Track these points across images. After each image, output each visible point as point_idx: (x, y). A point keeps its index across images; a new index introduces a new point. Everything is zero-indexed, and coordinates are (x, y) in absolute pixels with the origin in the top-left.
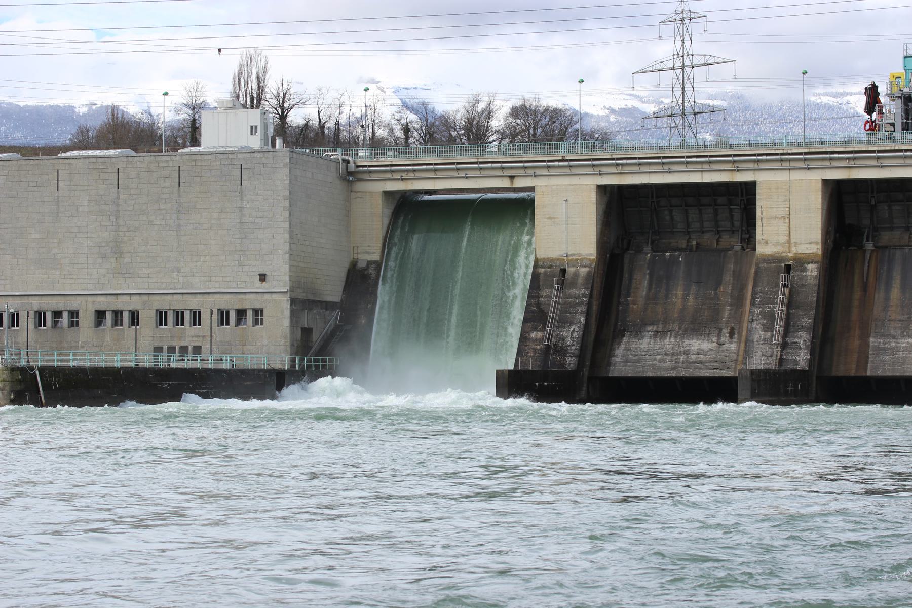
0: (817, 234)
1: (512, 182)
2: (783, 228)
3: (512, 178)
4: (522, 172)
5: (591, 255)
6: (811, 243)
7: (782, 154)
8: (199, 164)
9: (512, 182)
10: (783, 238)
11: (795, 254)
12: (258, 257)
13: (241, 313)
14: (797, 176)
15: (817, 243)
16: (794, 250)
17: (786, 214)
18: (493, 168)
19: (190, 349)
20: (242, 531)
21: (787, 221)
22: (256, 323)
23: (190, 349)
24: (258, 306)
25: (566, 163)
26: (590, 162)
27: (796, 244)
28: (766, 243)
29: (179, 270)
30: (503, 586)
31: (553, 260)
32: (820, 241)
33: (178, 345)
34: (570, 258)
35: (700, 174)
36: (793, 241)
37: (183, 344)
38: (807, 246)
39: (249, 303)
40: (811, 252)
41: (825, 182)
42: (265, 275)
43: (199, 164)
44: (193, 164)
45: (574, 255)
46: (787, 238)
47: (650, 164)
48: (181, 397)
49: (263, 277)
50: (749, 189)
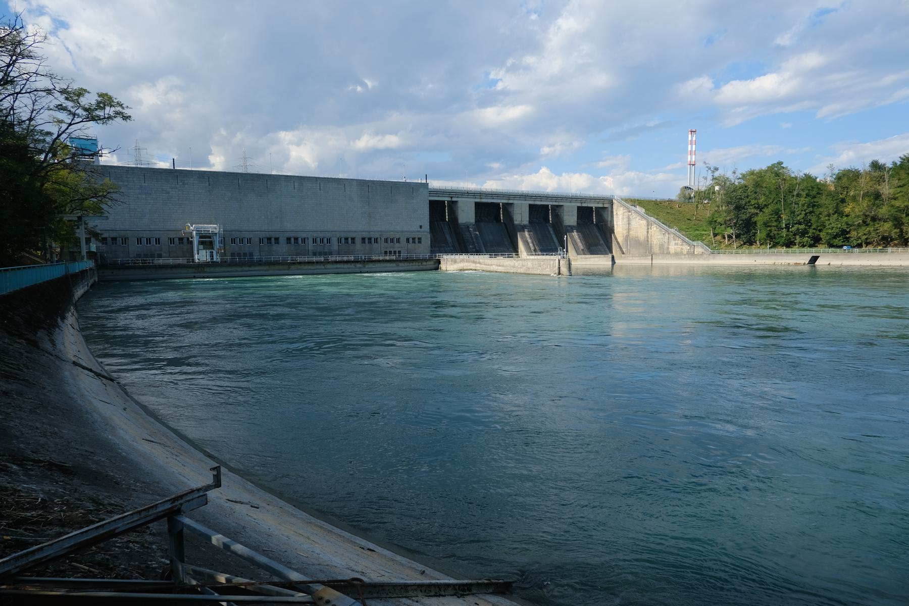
3: (582, 203)
4: (454, 196)
10: (520, 219)
31: (464, 223)
39: (417, 236)
49: (421, 227)
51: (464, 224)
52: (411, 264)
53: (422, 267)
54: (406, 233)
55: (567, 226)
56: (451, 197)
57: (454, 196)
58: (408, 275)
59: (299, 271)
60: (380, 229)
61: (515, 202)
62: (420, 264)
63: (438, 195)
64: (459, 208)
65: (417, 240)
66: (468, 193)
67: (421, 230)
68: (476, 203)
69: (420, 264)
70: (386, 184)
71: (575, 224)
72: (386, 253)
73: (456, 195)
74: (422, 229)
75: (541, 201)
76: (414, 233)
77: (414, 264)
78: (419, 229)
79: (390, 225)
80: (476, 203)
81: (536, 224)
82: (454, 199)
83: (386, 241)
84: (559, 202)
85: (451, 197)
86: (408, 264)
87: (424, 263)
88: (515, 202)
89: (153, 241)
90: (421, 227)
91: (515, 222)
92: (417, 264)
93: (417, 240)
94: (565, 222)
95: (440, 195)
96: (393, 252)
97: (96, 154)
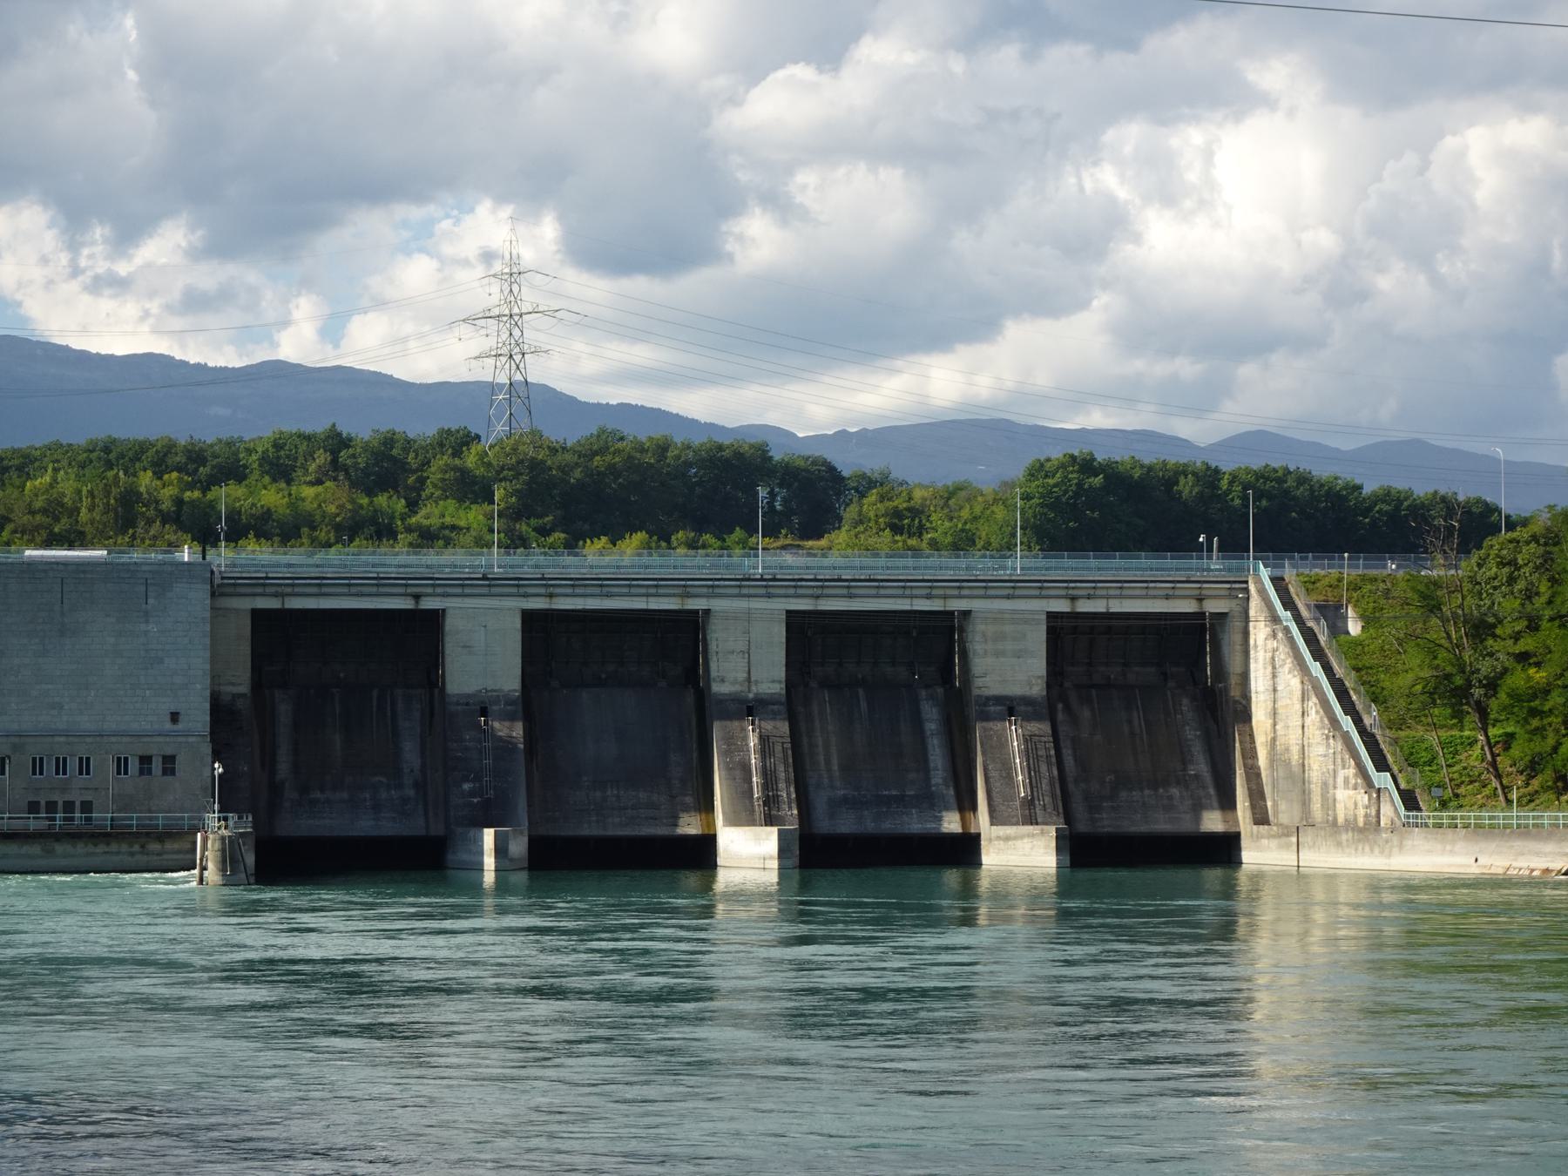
0: (781, 673)
1: (417, 603)
2: (743, 664)
3: (1073, 599)
4: (429, 590)
5: (515, 691)
6: (773, 681)
7: (826, 580)
8: (89, 576)
9: (417, 603)
10: (742, 676)
11: (756, 694)
12: (169, 692)
13: (145, 760)
14: (758, 604)
15: (780, 682)
16: (754, 688)
17: (745, 648)
18: (309, 585)
19: (78, 804)
20: (1446, 1054)
21: (747, 655)
22: (165, 772)
23: (78, 804)
24: (169, 751)
25: (764, 583)
26: (404, 582)
27: (756, 682)
28: (723, 681)
29: (62, 708)
30: (514, 1070)
31: (469, 696)
32: (784, 679)
33: (60, 799)
34: (490, 694)
35: (644, 599)
36: (752, 679)
37: (68, 798)
38: (771, 685)
39: (156, 749)
40: (773, 691)
41: (790, 614)
42: (178, 713)
43: (89, 576)
44: (82, 576)
45: (495, 691)
46: (745, 675)
47: (585, 586)
48: (1057, 879)
49: (175, 717)
50: (436, 617)
51: (466, 700)
52: (101, 848)
53: (145, 858)
54: (113, 739)
55: (988, 698)
56: (417, 597)
57: (429, 590)
58: (68, 878)
59: (142, 859)
60: (15, 727)
61: (717, 605)
62: (136, 848)
63: (354, 590)
64: (448, 639)
65: (157, 766)
66: (484, 578)
67: (175, 727)
68: (529, 617)
69: (136, 848)
70: (45, 571)
71: (1037, 689)
72: (33, 807)
73: (433, 586)
74: (180, 726)
75: (851, 596)
76: (145, 739)
77: (114, 847)
78: (168, 726)
79: (54, 712)
80: (529, 617)
81: (861, 692)
82: (428, 604)
83: (37, 766)
84: (945, 597)
85: (417, 597)
86: (91, 849)
87: (154, 846)
88: (717, 605)
89: (50, 767)
90: (175, 717)
91: (717, 688)
92: (124, 847)
93: (157, 766)
94: (978, 682)
95: (449, 590)
96: (43, 808)
97: (1359, 488)
